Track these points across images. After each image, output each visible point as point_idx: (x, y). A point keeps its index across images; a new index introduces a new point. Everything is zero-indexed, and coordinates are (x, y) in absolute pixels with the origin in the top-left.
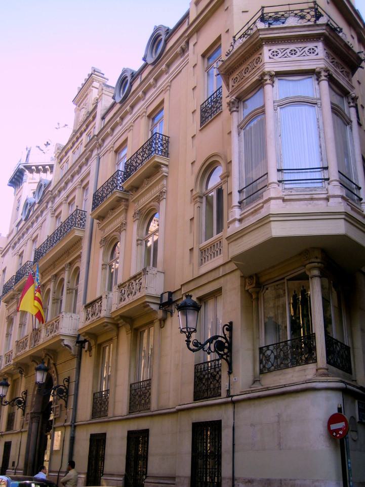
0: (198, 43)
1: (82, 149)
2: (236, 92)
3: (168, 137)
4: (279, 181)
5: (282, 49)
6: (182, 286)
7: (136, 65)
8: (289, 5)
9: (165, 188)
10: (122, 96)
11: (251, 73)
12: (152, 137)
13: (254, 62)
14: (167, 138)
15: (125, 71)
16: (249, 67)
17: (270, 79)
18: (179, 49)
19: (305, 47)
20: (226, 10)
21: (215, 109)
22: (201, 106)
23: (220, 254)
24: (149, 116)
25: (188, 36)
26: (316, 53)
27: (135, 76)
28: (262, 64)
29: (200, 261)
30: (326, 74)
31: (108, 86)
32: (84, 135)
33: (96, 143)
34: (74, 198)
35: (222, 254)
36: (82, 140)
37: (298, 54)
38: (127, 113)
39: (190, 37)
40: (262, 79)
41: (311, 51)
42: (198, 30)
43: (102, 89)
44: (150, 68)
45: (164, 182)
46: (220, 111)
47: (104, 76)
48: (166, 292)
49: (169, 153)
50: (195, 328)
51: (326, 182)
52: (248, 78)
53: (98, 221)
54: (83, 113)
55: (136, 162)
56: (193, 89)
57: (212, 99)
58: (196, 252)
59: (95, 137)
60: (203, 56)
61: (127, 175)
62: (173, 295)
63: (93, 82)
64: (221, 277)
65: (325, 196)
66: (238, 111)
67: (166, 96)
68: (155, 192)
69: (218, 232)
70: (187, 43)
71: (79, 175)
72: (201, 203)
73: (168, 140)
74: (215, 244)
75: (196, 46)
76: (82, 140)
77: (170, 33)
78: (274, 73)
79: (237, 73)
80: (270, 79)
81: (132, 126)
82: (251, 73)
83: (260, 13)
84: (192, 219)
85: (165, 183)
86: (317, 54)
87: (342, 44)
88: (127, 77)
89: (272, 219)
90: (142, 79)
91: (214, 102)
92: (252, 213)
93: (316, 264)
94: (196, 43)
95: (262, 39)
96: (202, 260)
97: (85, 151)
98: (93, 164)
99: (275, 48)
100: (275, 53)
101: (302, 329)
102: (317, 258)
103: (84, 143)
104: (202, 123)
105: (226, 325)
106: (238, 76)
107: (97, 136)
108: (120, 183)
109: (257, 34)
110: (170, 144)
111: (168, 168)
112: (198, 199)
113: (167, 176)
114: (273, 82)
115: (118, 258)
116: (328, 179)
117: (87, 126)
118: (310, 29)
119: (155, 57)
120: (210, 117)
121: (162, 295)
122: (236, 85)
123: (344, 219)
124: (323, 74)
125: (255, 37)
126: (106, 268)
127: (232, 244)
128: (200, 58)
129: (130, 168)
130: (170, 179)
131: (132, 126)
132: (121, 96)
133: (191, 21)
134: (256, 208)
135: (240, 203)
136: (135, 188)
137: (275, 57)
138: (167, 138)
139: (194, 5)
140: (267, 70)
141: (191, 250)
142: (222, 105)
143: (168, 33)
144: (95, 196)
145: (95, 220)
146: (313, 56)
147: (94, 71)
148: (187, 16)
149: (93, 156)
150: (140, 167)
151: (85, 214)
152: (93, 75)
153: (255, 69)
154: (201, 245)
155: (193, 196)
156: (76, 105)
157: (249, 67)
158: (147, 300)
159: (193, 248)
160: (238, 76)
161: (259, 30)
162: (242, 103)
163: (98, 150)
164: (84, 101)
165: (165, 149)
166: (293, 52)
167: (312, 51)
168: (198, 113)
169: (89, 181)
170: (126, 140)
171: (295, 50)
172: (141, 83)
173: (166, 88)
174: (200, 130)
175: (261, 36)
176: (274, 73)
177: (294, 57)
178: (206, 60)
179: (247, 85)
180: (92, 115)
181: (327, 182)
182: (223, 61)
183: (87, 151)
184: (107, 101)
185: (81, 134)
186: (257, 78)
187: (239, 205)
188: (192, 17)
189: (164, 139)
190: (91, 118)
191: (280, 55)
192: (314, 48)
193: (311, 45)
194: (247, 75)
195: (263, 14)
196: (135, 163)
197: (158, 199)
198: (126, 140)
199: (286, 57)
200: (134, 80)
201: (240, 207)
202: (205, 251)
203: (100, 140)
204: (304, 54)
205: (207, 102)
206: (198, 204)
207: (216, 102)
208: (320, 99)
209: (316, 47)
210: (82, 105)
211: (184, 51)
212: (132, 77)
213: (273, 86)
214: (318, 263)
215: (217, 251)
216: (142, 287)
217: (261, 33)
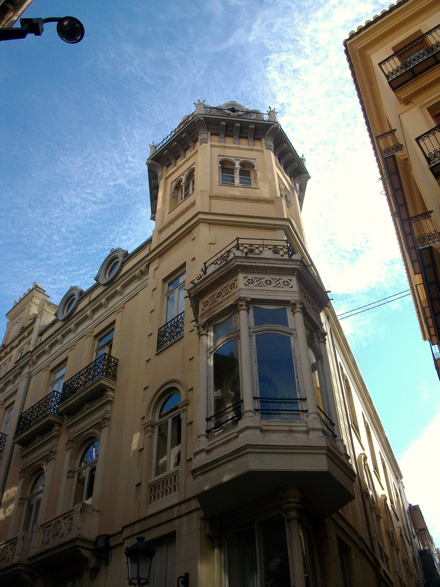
0: (160, 268)
1: (11, 365)
2: (207, 315)
3: (117, 360)
4: (255, 410)
5: (214, 302)
6: (124, 528)
7: (85, 282)
8: (263, 239)
9: (109, 415)
10: (66, 314)
11: (225, 298)
12: (96, 360)
13: (229, 287)
14: (116, 360)
16: (222, 292)
17: (245, 305)
18: (137, 272)
19: (280, 279)
20: (193, 240)
21: (175, 334)
22: (159, 330)
23: (175, 491)
24: (96, 337)
27: (83, 295)
28: (237, 289)
29: (149, 498)
30: (301, 306)
31: (49, 304)
32: (15, 352)
33: (29, 360)
34: (13, 403)
35: (177, 492)
36: (12, 356)
37: (273, 284)
38: (70, 331)
39: (151, 261)
40: (237, 304)
41: (286, 283)
42: (160, 255)
43: (44, 305)
44: (100, 290)
45: (108, 407)
46: (181, 336)
47: (45, 293)
48: (102, 536)
49: (117, 376)
50: (146, 578)
51: (304, 414)
52: (221, 302)
53: (20, 447)
54: (17, 328)
55: (78, 383)
56: (151, 312)
57: (173, 323)
58: (144, 488)
59: (29, 354)
60: (164, 280)
61: (64, 397)
62: (111, 540)
63: (33, 297)
64: (175, 519)
65: (305, 429)
67: (117, 317)
68: (45, 449)
70: (148, 266)
71: (3, 394)
72: (153, 432)
73: (117, 362)
74: (169, 480)
75: (157, 271)
76: (12, 356)
77: (128, 257)
79: (209, 296)
80: (245, 305)
81: (75, 345)
82: (225, 298)
83: (235, 243)
85: (109, 409)
86: (292, 287)
88: (74, 295)
89: (248, 450)
90: (92, 299)
91: (174, 327)
92: (224, 443)
93: (294, 505)
94: (158, 267)
95: (238, 266)
96: (151, 498)
97: (15, 366)
98: (21, 383)
99: (250, 276)
100: (251, 281)
103: (14, 359)
104: (159, 347)
105: (181, 577)
106: (209, 300)
107: (32, 352)
108: (55, 405)
109: (234, 261)
110: (118, 367)
111: (114, 393)
112: (149, 428)
113: (112, 401)
114: (249, 309)
115: (41, 492)
116: (307, 411)
117: (20, 342)
118: (286, 263)
119: (108, 279)
120: (169, 342)
121: (97, 538)
122: (207, 308)
123: (326, 454)
124: (298, 306)
125: (232, 263)
126: (73, 477)
128: (160, 282)
129: (69, 389)
130: (115, 404)
131: (75, 345)
132: (65, 313)
133: (152, 248)
134: (229, 438)
135: (208, 431)
136: (71, 412)
137: (251, 285)
138: (116, 360)
139: (156, 233)
141: (139, 485)
142: (183, 330)
143: (126, 256)
144: (21, 418)
145: (16, 445)
147: (36, 286)
148: (149, 241)
149: (23, 374)
150: (82, 388)
151: (4, 437)
152: (34, 290)
153: (215, 304)
154: (151, 481)
156: (10, 319)
157: (222, 292)
158: (78, 543)
159: (140, 484)
160: (209, 300)
161: (236, 257)
162: (212, 327)
163: (30, 368)
164: (19, 316)
165: (113, 372)
166: (268, 282)
167: (286, 283)
168: (155, 337)
169: (15, 401)
170: (66, 359)
171: (270, 281)
172: (90, 303)
173: (120, 309)
174: (156, 355)
175: (238, 263)
176: (249, 299)
177: (269, 287)
178: (167, 285)
179: (219, 310)
180: (26, 330)
181: (305, 414)
182: (195, 284)
183: (17, 368)
184: (48, 318)
185: (12, 349)
186: (232, 302)
187: (206, 434)
188: (154, 245)
189: (112, 361)
190: (26, 334)
192: (289, 281)
193: (285, 278)
194: (220, 300)
195: (238, 244)
196: (77, 384)
197: (99, 426)
198: (66, 359)
199: (261, 286)
200: (82, 298)
201: (207, 437)
202: (155, 487)
203: (34, 358)
204: (279, 285)
205: (176, 319)
206: (149, 434)
207: (177, 327)
208: (295, 330)
209: (291, 280)
210: (17, 319)
211: (143, 273)
212: (80, 295)
213: (248, 313)
214: (296, 503)
215: (171, 488)
216: (16, 554)
217: (238, 260)
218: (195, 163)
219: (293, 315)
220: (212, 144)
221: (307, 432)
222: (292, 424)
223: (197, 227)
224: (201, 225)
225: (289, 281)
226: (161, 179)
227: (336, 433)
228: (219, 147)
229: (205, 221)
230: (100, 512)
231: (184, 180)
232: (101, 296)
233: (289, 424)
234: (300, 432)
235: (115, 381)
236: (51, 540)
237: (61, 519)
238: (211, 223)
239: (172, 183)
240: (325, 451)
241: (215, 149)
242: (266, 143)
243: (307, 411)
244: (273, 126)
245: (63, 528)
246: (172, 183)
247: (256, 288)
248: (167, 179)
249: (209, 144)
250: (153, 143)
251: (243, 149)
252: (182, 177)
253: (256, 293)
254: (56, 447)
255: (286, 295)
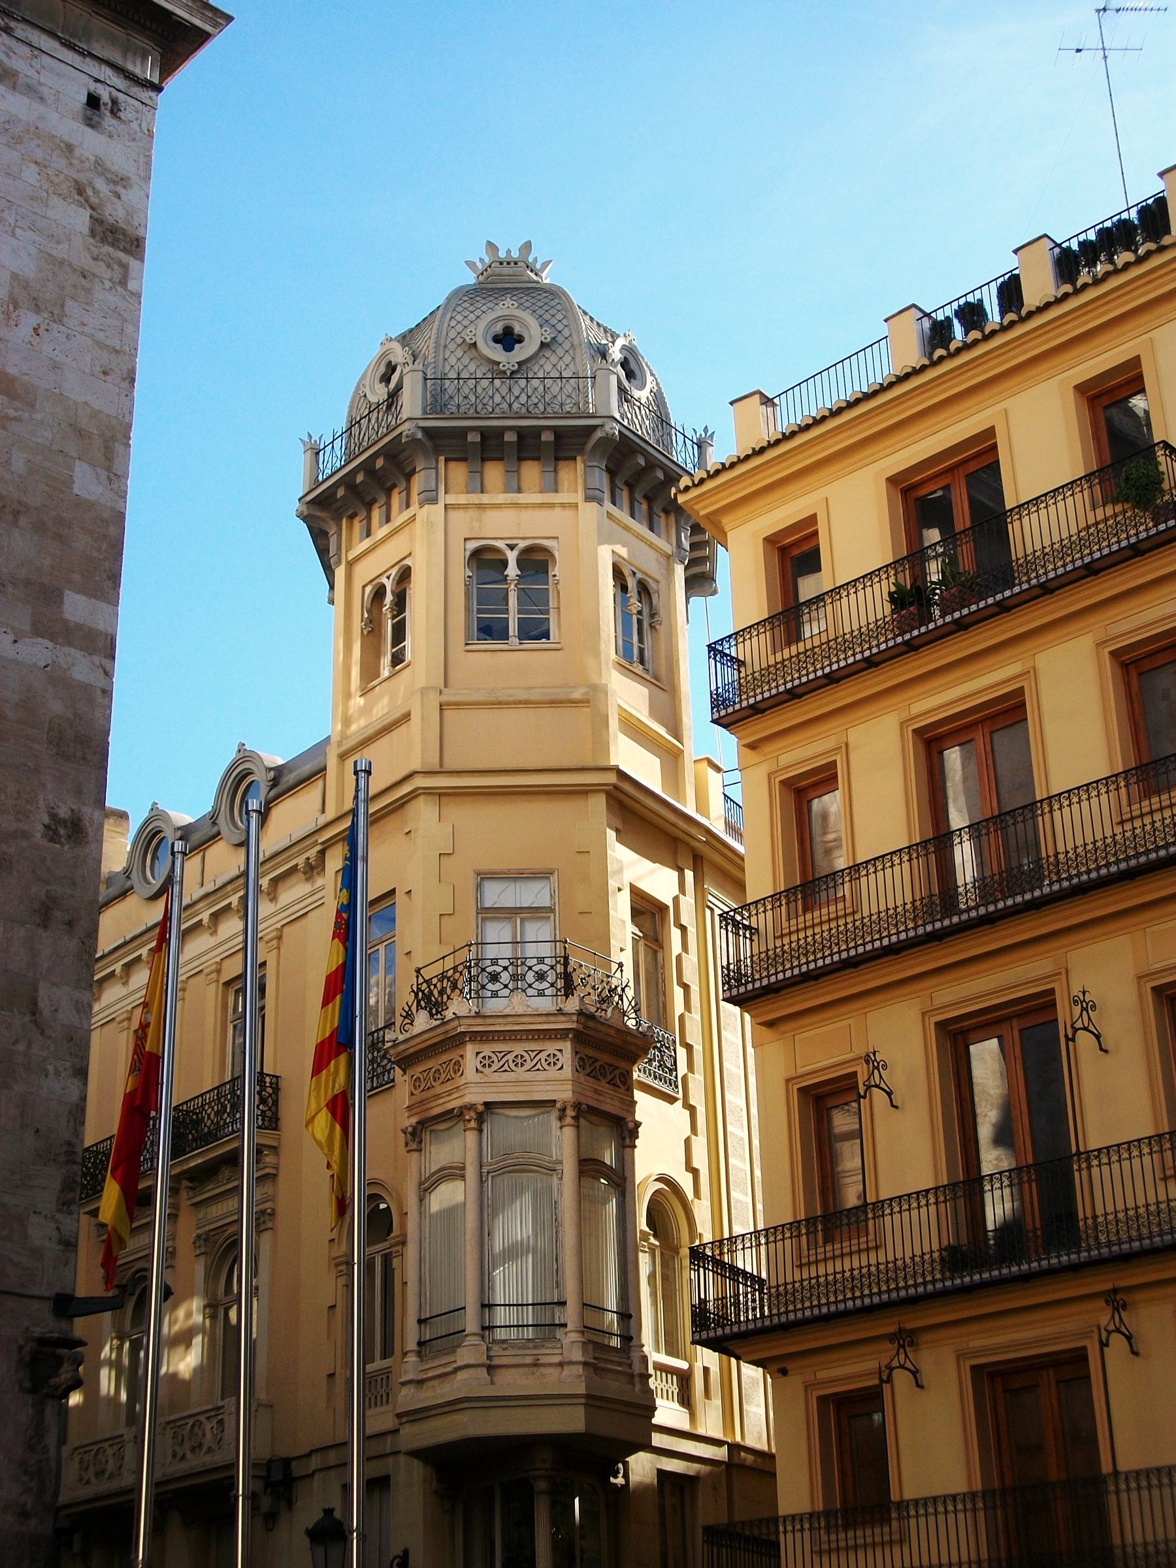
3: (277, 1077)
15: (244, 756)
18: (300, 861)
25: (322, 843)
26: (559, 1066)
41: (552, 1061)
64: (388, 1455)
65: (556, 1359)
66: (420, 1151)
69: (384, 1356)
70: (322, 853)
73: (277, 1084)
78: (481, 1108)
84: (333, 1307)
86: (562, 1068)
87: (613, 1032)
99: (487, 1050)
101: (577, 1500)
102: (544, 1461)
110: (281, 1095)
116: (565, 1325)
118: (552, 1019)
127: (407, 1425)
137: (487, 1070)
138: (274, 1080)
140: (469, 1099)
146: (552, 1072)
155: (334, 1259)
159: (333, 1374)
166: (519, 1061)
177: (521, 1073)
191: (495, 1067)
193: (551, 1047)
201: (419, 1354)
208: (561, 1162)
209: (560, 1051)
214: (546, 1469)
217: (462, 1021)
218: (410, 554)
219: (561, 1128)
220: (451, 499)
221: (561, 1365)
222: (539, 1352)
223: (413, 802)
224: (421, 799)
225: (557, 1053)
226: (339, 563)
227: (633, 1333)
228: (465, 507)
229: (428, 792)
230: (271, 1406)
231: (389, 585)
232: (229, 888)
233: (535, 1352)
234: (550, 1365)
235: (276, 1129)
236: (188, 1455)
237: (202, 1418)
238: (442, 795)
239: (364, 587)
240: (583, 1401)
241: (454, 515)
242: (585, 481)
243: (565, 1325)
244: (599, 434)
245: (209, 1435)
246: (364, 587)
247: (497, 1077)
248: (351, 564)
249: (441, 505)
250: (310, 436)
251: (527, 506)
252: (384, 580)
253: (495, 1090)
254: (174, 1239)
255: (549, 1088)
